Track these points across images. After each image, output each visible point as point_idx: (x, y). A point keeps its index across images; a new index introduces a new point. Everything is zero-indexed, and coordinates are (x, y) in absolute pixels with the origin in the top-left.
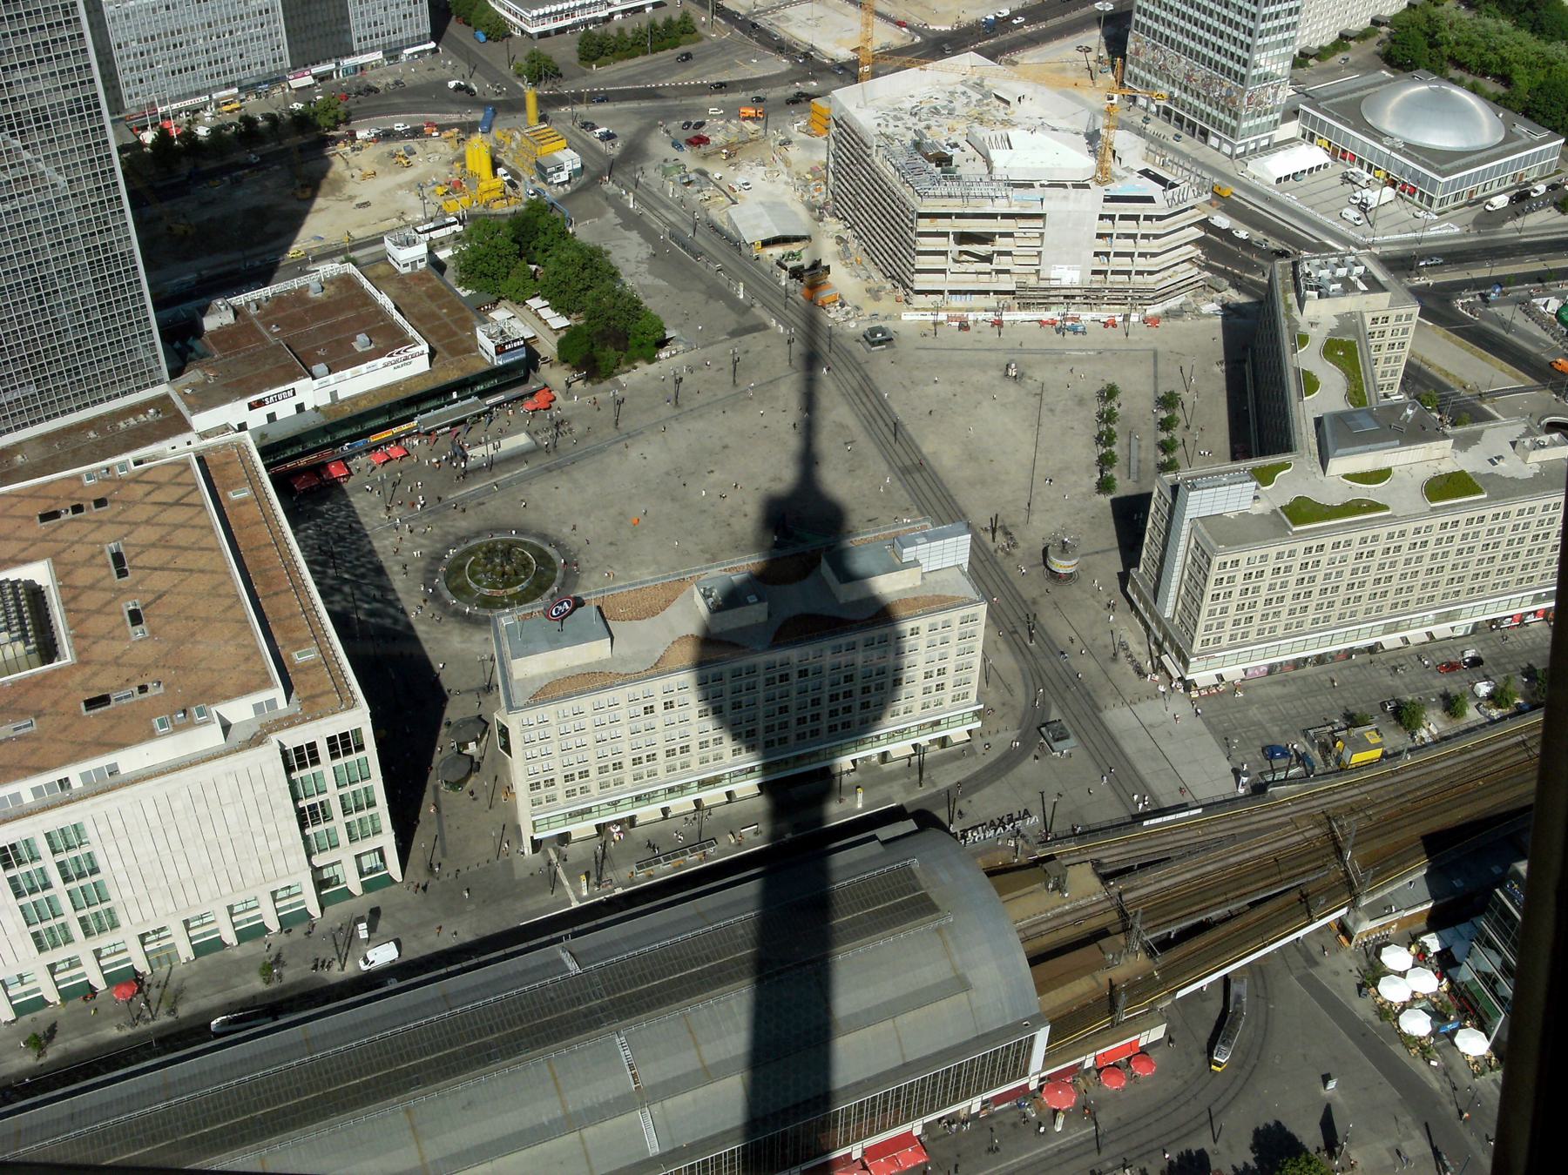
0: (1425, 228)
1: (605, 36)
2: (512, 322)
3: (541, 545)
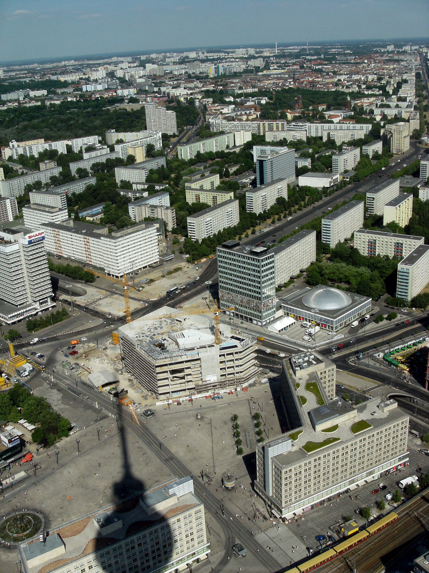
0: (332, 338)
1: (36, 321)
2: (13, 430)
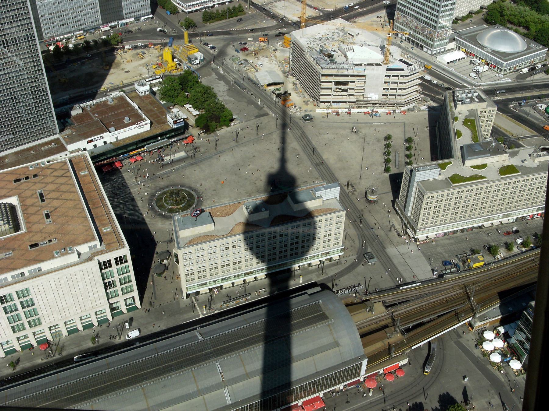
0: (499, 80)
1: (212, 13)
2: (179, 112)
3: (189, 191)
